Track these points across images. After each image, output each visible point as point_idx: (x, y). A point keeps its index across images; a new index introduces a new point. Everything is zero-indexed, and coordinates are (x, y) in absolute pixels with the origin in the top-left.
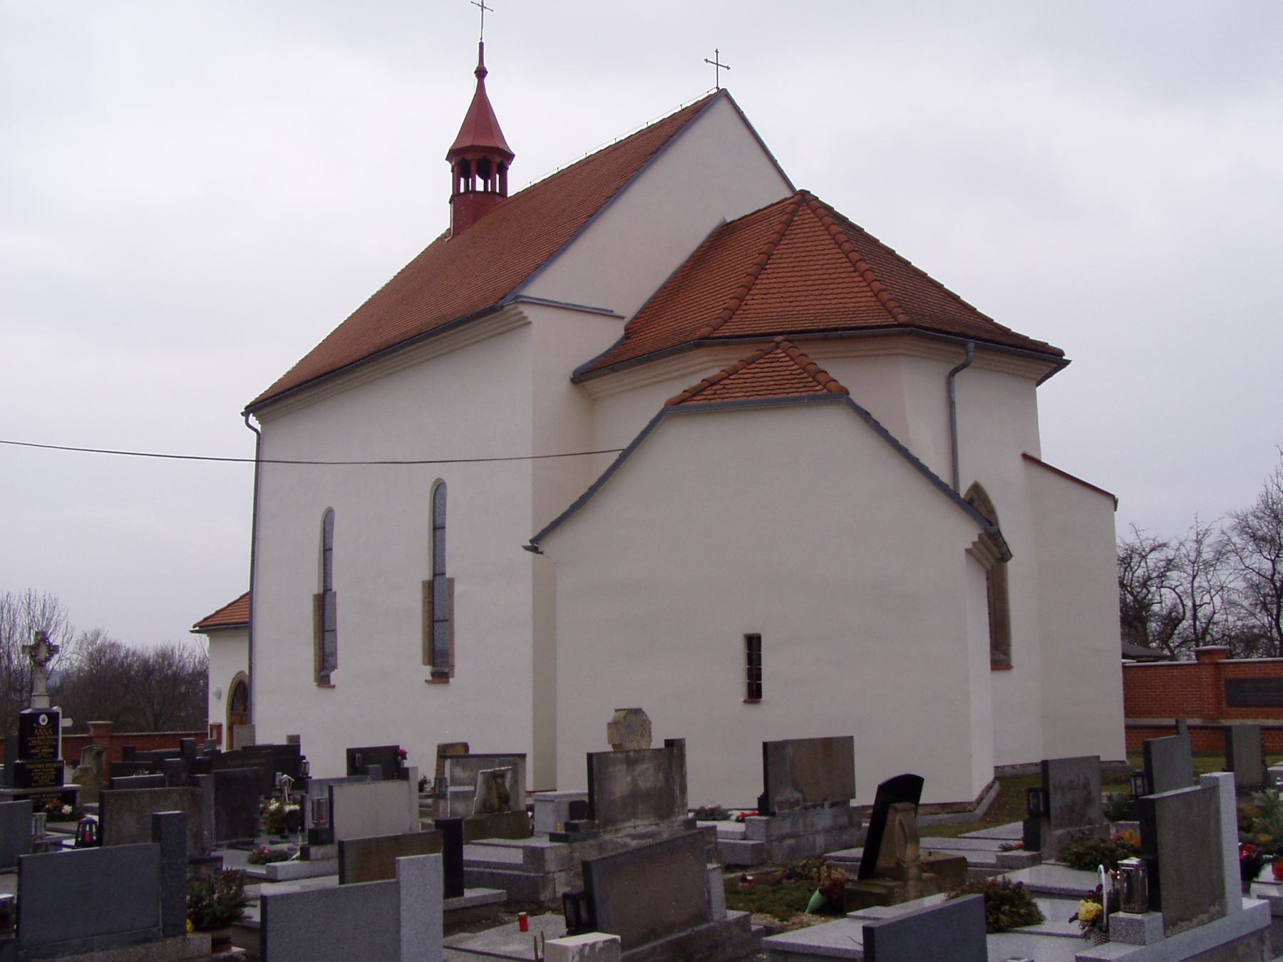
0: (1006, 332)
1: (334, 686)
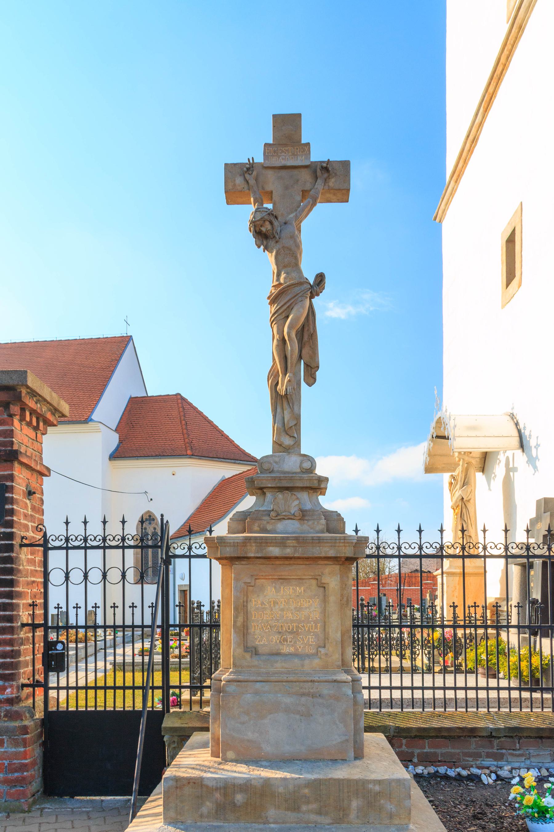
0: (243, 452)
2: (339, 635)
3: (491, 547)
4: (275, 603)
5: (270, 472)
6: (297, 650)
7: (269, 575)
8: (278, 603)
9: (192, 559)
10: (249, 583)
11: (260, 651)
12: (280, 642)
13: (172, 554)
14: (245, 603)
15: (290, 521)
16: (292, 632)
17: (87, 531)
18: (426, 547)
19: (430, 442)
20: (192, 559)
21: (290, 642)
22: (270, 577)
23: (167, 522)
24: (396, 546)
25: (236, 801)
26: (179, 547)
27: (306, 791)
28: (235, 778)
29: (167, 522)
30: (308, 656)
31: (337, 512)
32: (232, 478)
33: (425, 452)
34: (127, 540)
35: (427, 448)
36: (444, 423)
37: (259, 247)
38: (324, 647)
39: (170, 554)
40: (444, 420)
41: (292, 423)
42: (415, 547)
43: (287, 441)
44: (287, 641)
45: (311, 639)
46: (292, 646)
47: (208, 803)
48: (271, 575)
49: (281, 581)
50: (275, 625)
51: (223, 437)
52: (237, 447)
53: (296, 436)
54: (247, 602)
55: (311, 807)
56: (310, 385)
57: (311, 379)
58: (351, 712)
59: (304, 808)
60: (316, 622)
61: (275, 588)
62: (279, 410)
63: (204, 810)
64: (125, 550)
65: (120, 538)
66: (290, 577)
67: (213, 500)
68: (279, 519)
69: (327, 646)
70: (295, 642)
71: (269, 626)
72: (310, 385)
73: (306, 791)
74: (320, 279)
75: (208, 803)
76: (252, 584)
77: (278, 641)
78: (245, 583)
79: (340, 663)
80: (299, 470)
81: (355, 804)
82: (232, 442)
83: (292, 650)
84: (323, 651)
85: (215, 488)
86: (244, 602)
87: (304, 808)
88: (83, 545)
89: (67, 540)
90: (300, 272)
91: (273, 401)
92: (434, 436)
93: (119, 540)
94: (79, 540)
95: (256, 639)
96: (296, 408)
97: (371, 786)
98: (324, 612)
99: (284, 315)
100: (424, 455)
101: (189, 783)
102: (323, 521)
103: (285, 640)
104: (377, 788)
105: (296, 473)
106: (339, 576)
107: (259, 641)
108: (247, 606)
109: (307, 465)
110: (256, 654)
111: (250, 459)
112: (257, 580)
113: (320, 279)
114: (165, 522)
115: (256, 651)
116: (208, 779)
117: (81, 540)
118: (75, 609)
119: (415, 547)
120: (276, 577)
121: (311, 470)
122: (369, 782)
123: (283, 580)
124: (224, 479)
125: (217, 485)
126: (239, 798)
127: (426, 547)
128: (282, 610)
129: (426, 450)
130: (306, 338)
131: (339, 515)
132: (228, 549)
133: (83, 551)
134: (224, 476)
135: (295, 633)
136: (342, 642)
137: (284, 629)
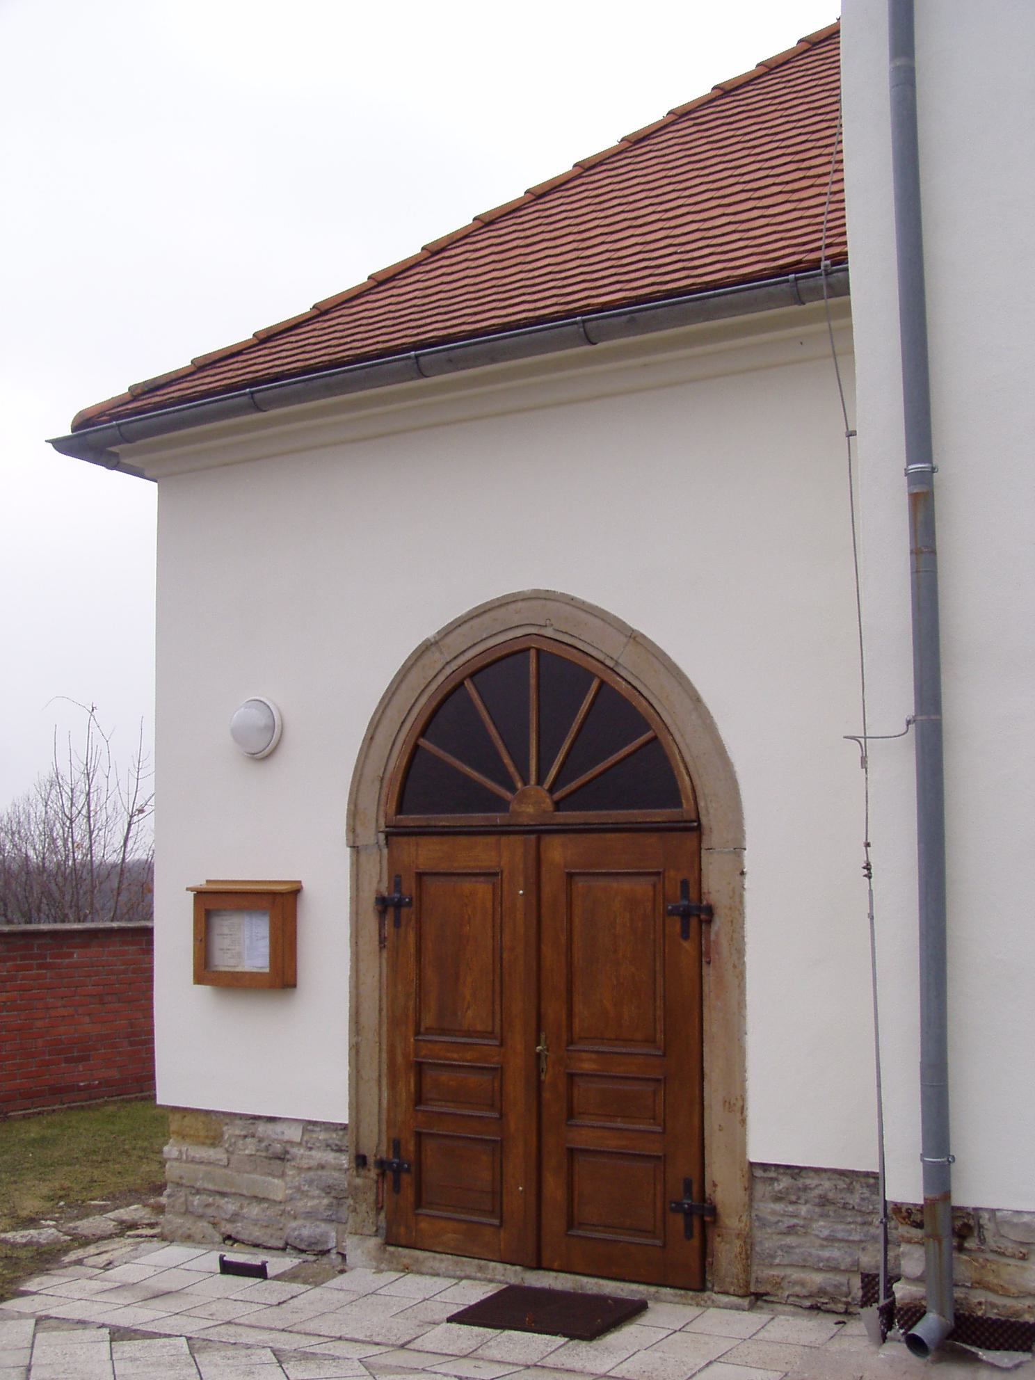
1: (188, 889)
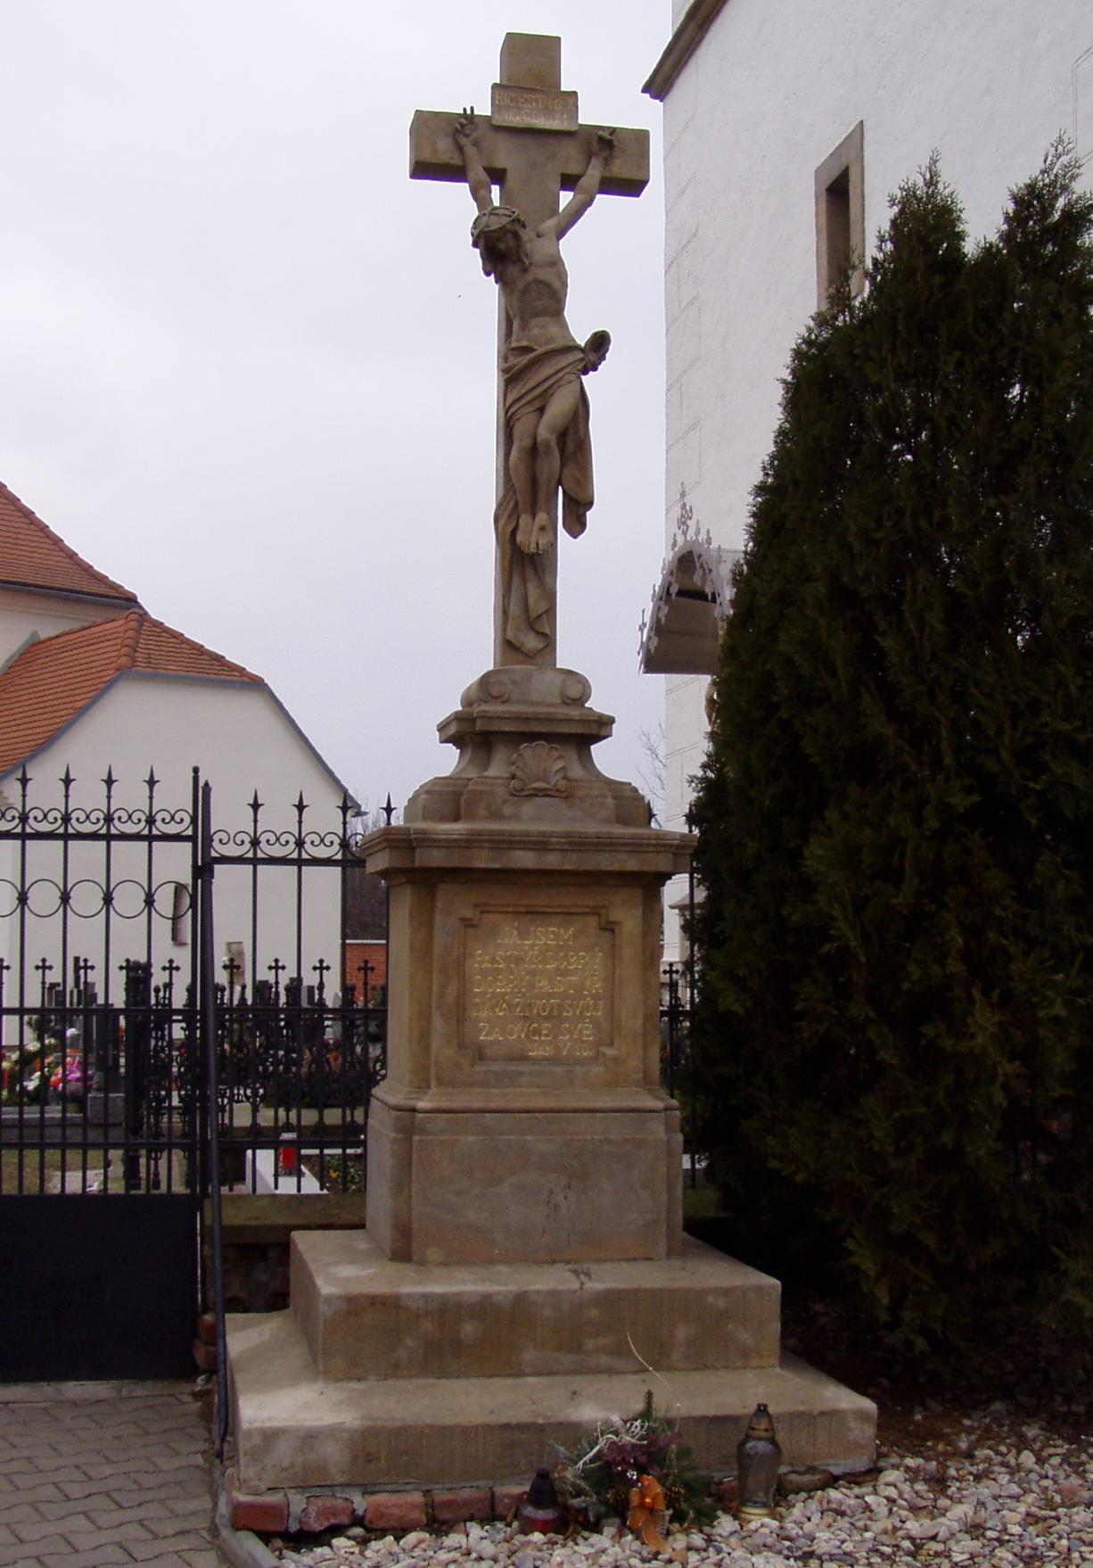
2: (639, 1022)
3: (268, 841)
4: (519, 960)
5: (503, 702)
6: (558, 1050)
7: (509, 905)
8: (523, 960)
9: (304, 868)
10: (470, 919)
11: (489, 1052)
12: (527, 1036)
13: (217, 855)
14: (461, 959)
15: (548, 799)
16: (547, 1018)
17: (27, 799)
18: (312, 842)
19: (662, 603)
20: (304, 868)
21: (546, 1035)
22: (510, 909)
23: (207, 784)
24: (292, 840)
25: (462, 1336)
26: (232, 841)
27: (594, 1313)
28: (459, 1294)
29: (207, 784)
30: (581, 1062)
31: (630, 784)
32: (59, 640)
33: (644, 624)
34: (116, 822)
35: (652, 618)
36: (702, 566)
37: (488, 274)
38: (611, 1044)
39: (214, 854)
40: (702, 559)
41: (543, 607)
42: (332, 843)
43: (532, 642)
44: (540, 1035)
45: (587, 1032)
46: (549, 1043)
47: (409, 1342)
48: (514, 905)
49: (529, 916)
50: (518, 1004)
51: (32, 527)
52: (87, 570)
53: (548, 631)
54: (464, 958)
55: (602, 1341)
56: (575, 535)
57: (577, 524)
58: (662, 1168)
59: (590, 1344)
60: (596, 997)
61: (518, 929)
62: (516, 581)
63: (402, 1353)
64: (27, 842)
65: (101, 816)
66: (547, 910)
67: (6, 696)
68: (526, 796)
69: (615, 1044)
70: (555, 1037)
71: (504, 1006)
72: (575, 535)
73: (594, 1313)
74: (600, 343)
75: (409, 1342)
76: (475, 923)
77: (523, 1035)
78: (462, 919)
79: (640, 1076)
80: (558, 701)
81: (682, 1333)
82: (57, 542)
83: (547, 1051)
84: (609, 1052)
85: (10, 664)
86: (459, 957)
87: (590, 1344)
88: (19, 830)
89: (151, 821)
90: (564, 326)
91: (506, 563)
92: (674, 590)
93: (56, 819)
94: (178, 820)
95: (482, 1030)
96: (548, 579)
97: (710, 1299)
98: (611, 978)
99: (537, 404)
100: (641, 629)
101: (373, 1304)
102: (610, 801)
103: (537, 1032)
104: (722, 1303)
105: (553, 705)
106: (641, 908)
107: (486, 1036)
108: (464, 966)
109: (574, 692)
110: (480, 1059)
111: (112, 593)
112: (486, 915)
113: (600, 343)
114: (201, 783)
115: (480, 1055)
116: (409, 1295)
117: (14, 818)
118: (40, 971)
119: (332, 843)
120: (522, 909)
121: (580, 701)
122: (707, 1292)
123: (536, 914)
124: (36, 640)
125: (16, 657)
126: (469, 1329)
127: (268, 841)
128: (532, 973)
129: (647, 619)
130: (570, 447)
131: (636, 790)
132: (435, 853)
133: (61, 843)
134: (35, 634)
135: (555, 1017)
136: (644, 1035)
137: (535, 1011)
